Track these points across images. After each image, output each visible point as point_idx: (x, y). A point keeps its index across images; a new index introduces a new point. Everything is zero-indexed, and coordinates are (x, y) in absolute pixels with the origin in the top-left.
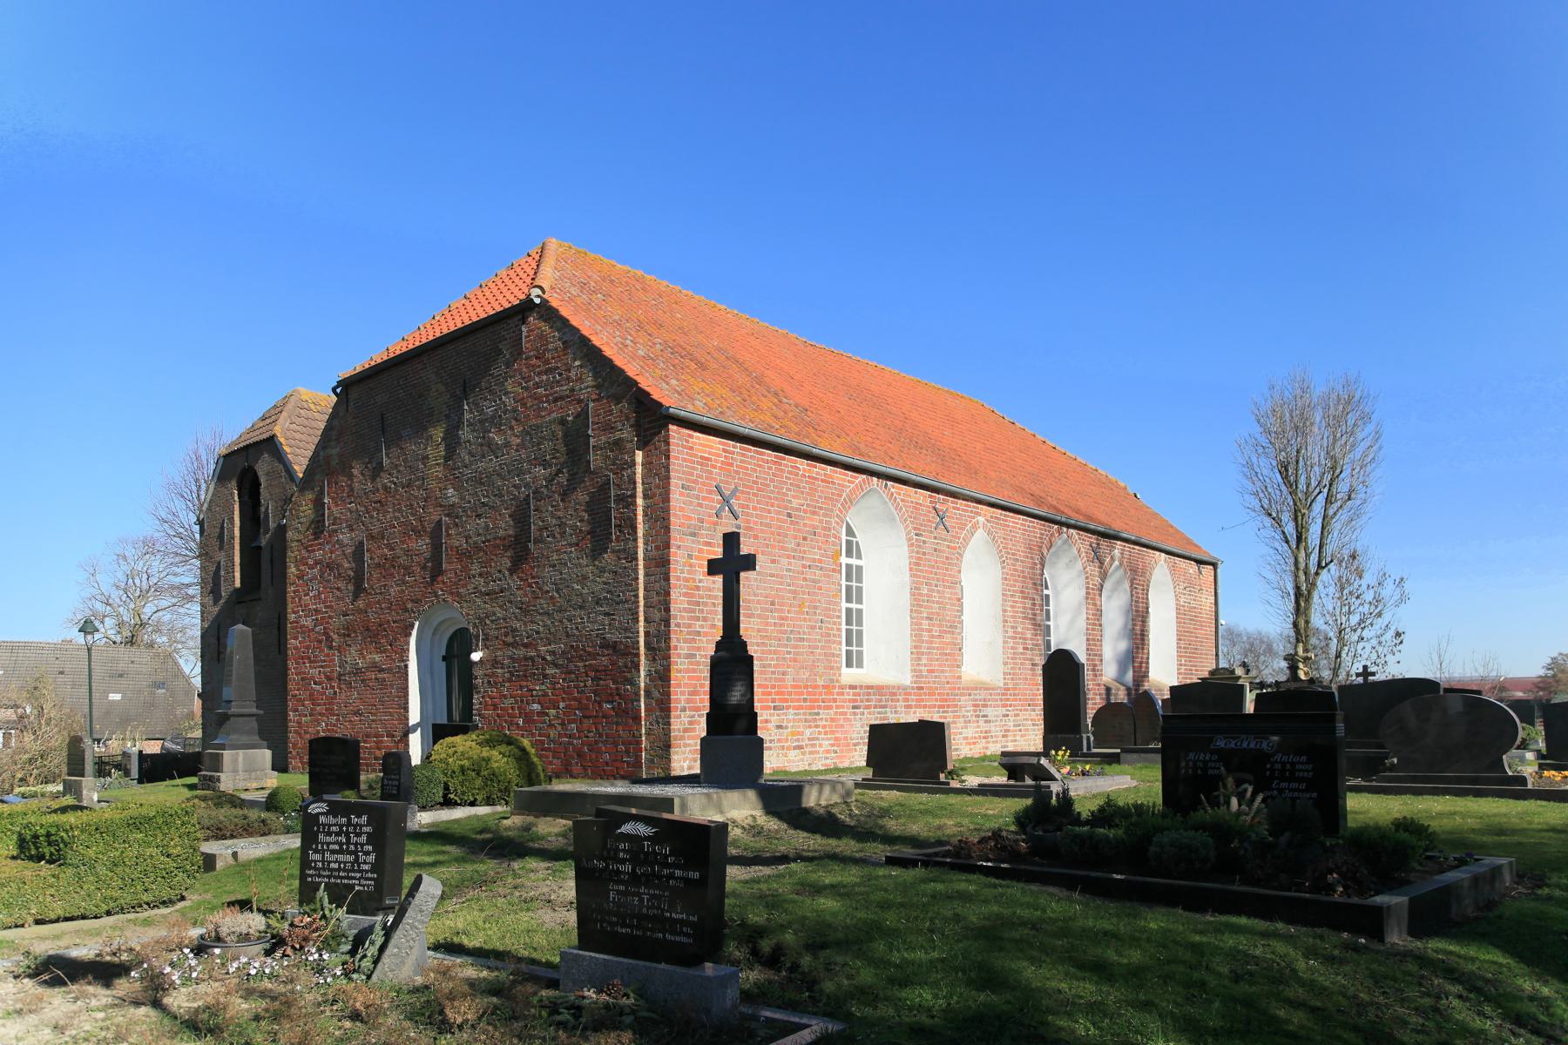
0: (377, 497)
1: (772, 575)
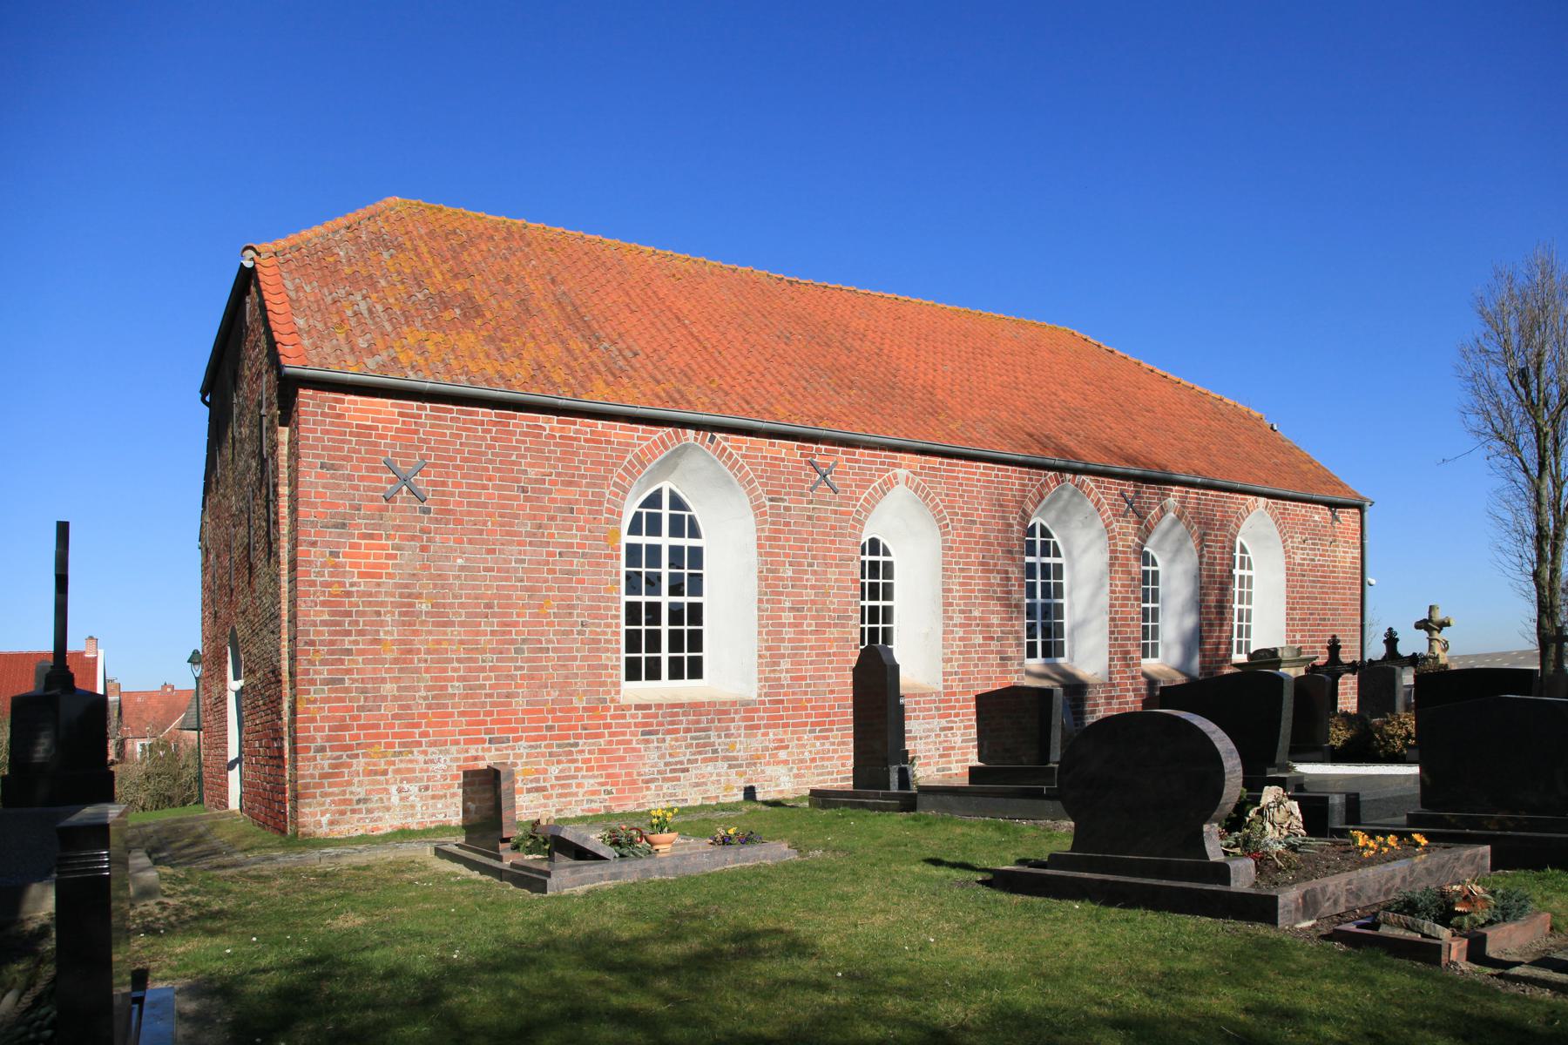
1: (487, 569)
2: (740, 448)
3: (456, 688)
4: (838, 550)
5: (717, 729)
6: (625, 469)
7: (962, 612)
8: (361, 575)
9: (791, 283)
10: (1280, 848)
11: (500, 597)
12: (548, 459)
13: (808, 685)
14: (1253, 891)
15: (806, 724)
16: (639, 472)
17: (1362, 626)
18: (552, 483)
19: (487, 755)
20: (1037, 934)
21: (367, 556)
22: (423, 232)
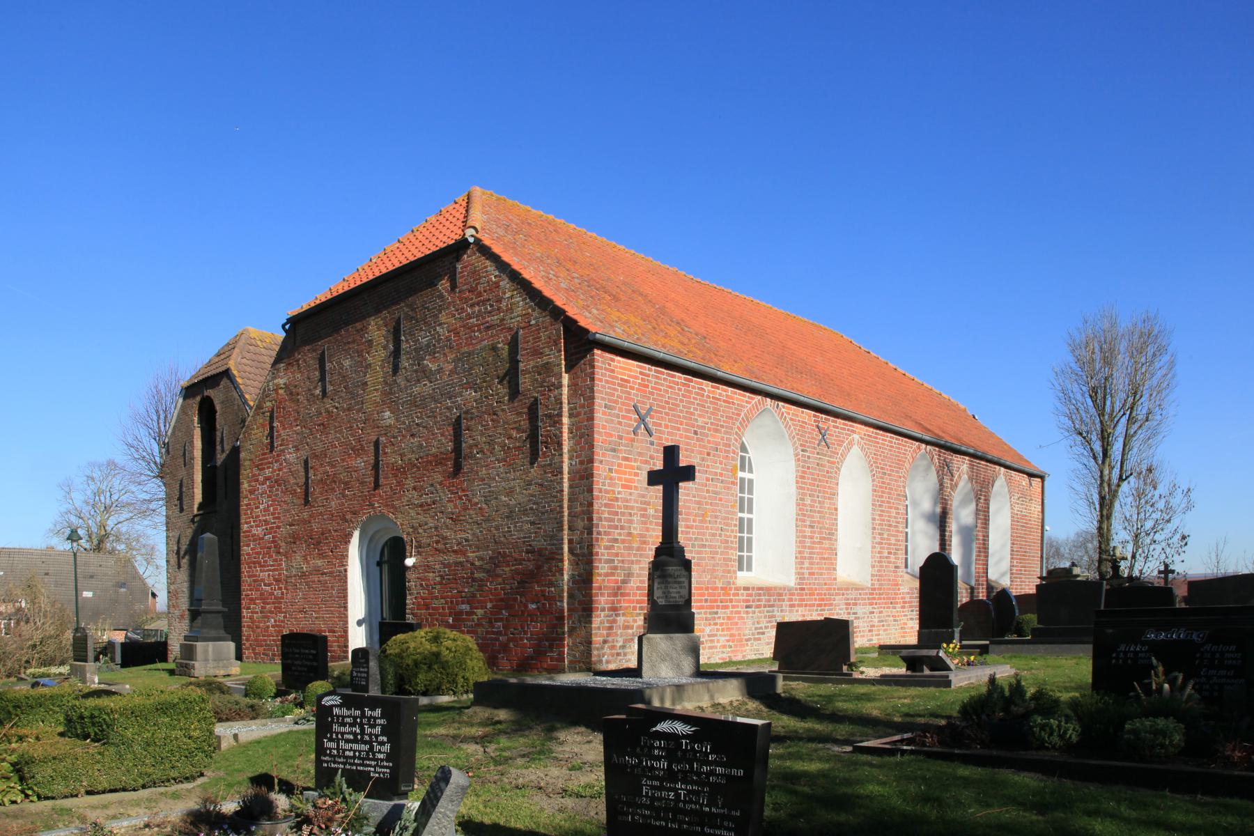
0: (320, 420)
18: (709, 429)
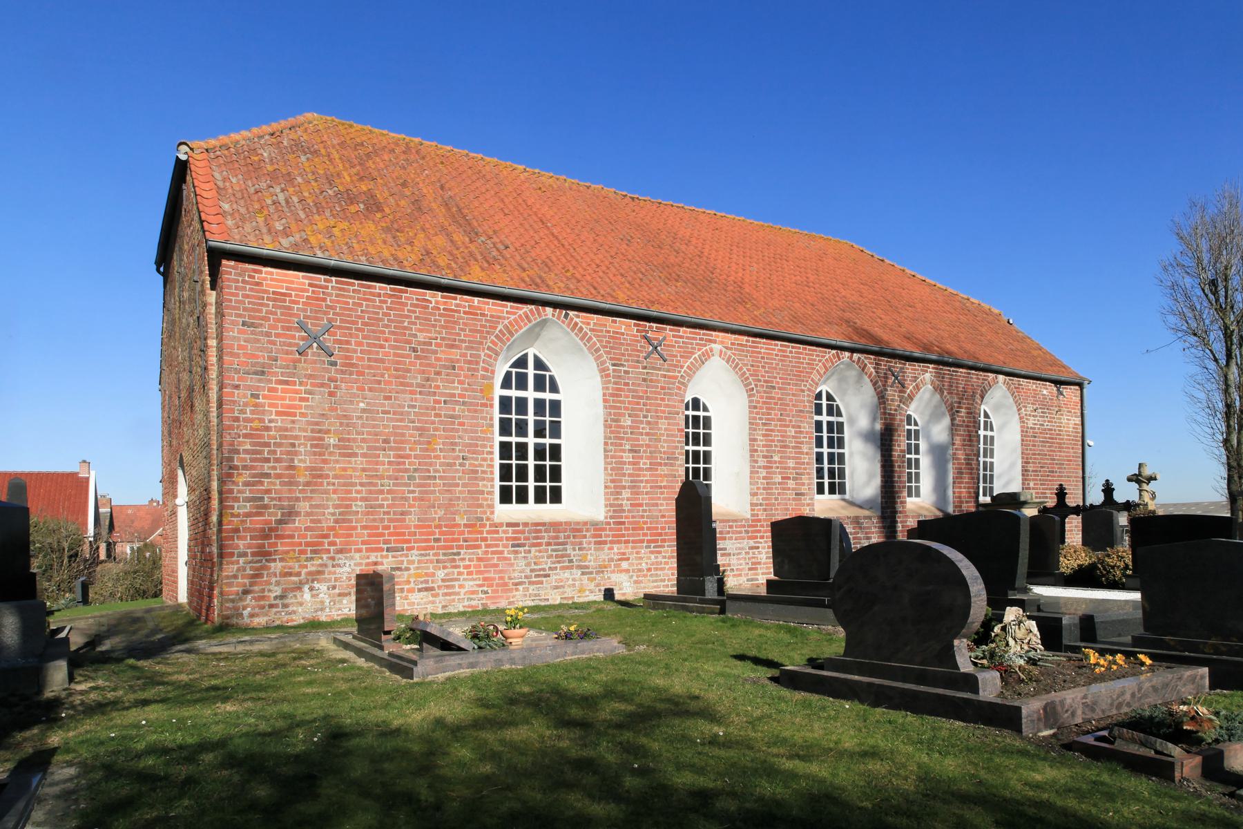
1: (384, 412)
2: (588, 324)
3: (358, 506)
4: (667, 406)
5: (572, 543)
6: (497, 336)
7: (764, 457)
8: (278, 413)
9: (633, 199)
10: (1022, 662)
11: (396, 434)
12: (434, 326)
13: (644, 511)
14: (999, 701)
15: (642, 541)
16: (508, 339)
17: (1083, 478)
18: (438, 345)
19: (385, 561)
20: (812, 731)
21: (283, 399)
22: (335, 142)
